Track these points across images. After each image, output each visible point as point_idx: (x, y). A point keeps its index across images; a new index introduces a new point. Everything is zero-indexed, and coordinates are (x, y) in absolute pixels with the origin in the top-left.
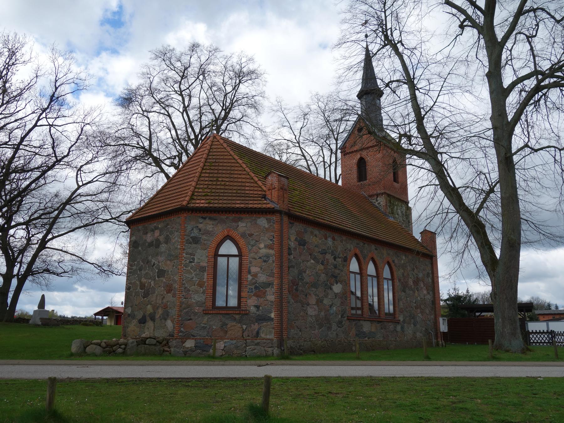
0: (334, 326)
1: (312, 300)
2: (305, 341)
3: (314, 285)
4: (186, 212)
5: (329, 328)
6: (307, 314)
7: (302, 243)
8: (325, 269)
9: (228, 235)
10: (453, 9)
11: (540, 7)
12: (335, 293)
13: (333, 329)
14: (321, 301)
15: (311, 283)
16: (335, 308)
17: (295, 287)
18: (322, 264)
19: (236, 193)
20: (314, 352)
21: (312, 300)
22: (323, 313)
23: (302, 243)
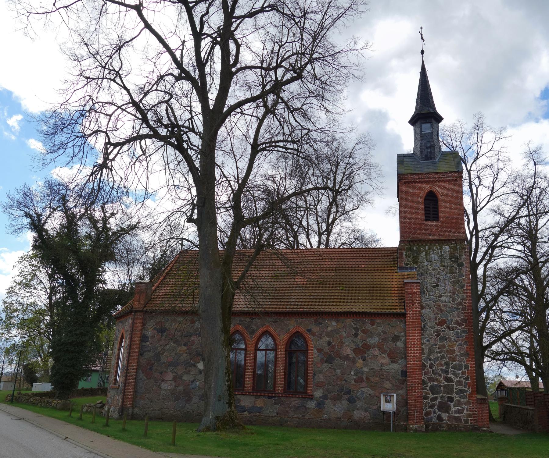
0: (195, 399)
1: (169, 376)
2: (153, 410)
3: (174, 364)
4: (379, 316)
5: (189, 400)
6: (160, 388)
7: (162, 331)
8: (188, 349)
9: (267, 331)
10: (235, 50)
11: (207, 6)
12: (200, 370)
13: (193, 402)
14: (181, 377)
15: (169, 363)
16: (198, 383)
17: (149, 367)
18: (185, 345)
19: (342, 290)
20: (163, 419)
21: (169, 376)
22: (181, 388)
23: (162, 331)
